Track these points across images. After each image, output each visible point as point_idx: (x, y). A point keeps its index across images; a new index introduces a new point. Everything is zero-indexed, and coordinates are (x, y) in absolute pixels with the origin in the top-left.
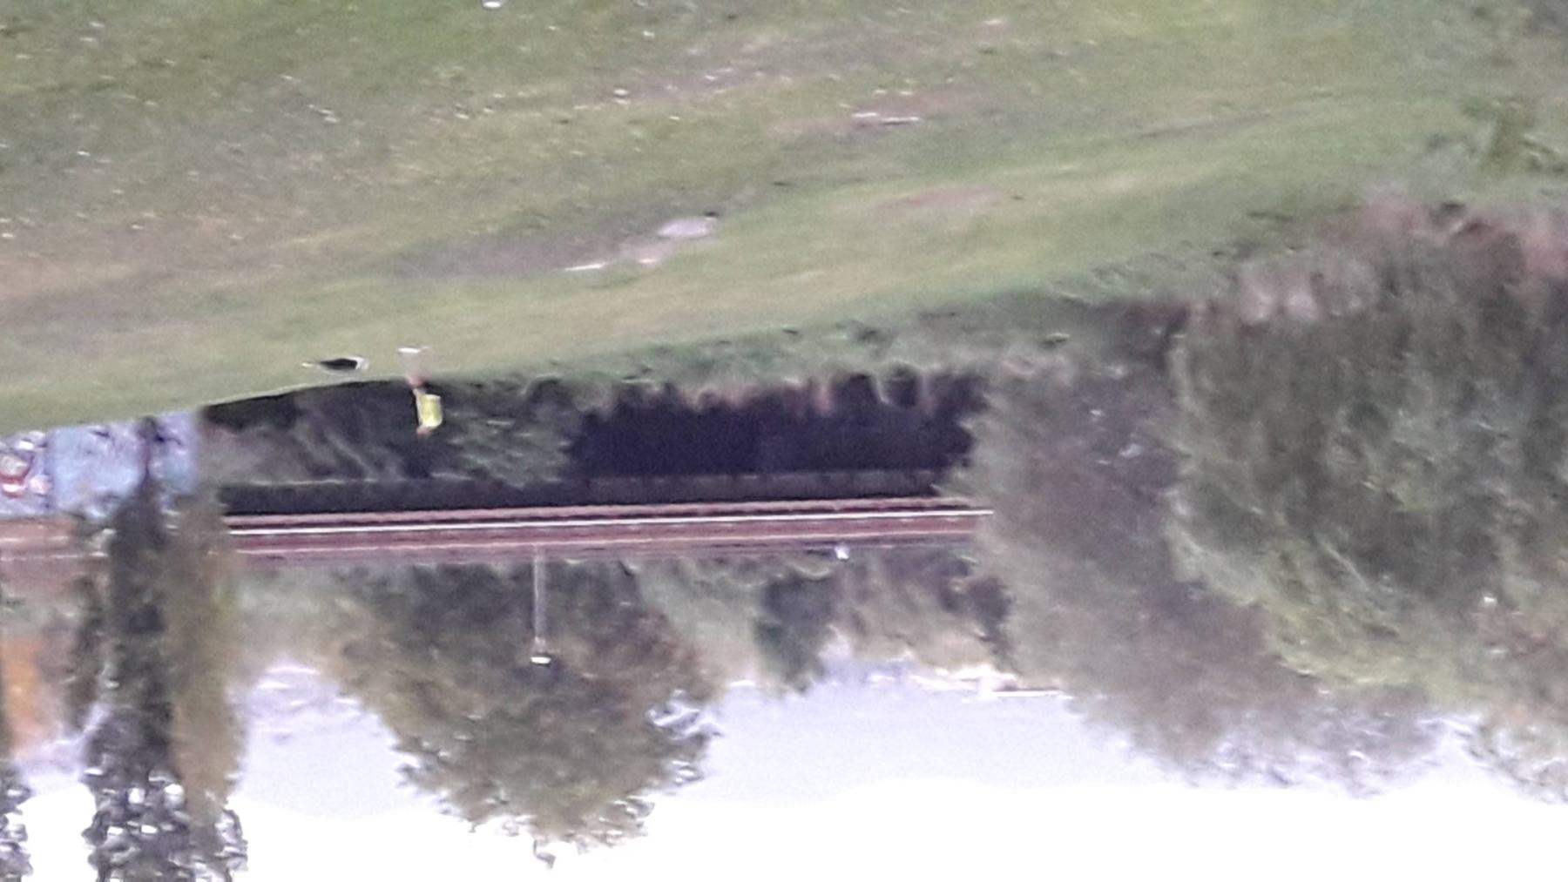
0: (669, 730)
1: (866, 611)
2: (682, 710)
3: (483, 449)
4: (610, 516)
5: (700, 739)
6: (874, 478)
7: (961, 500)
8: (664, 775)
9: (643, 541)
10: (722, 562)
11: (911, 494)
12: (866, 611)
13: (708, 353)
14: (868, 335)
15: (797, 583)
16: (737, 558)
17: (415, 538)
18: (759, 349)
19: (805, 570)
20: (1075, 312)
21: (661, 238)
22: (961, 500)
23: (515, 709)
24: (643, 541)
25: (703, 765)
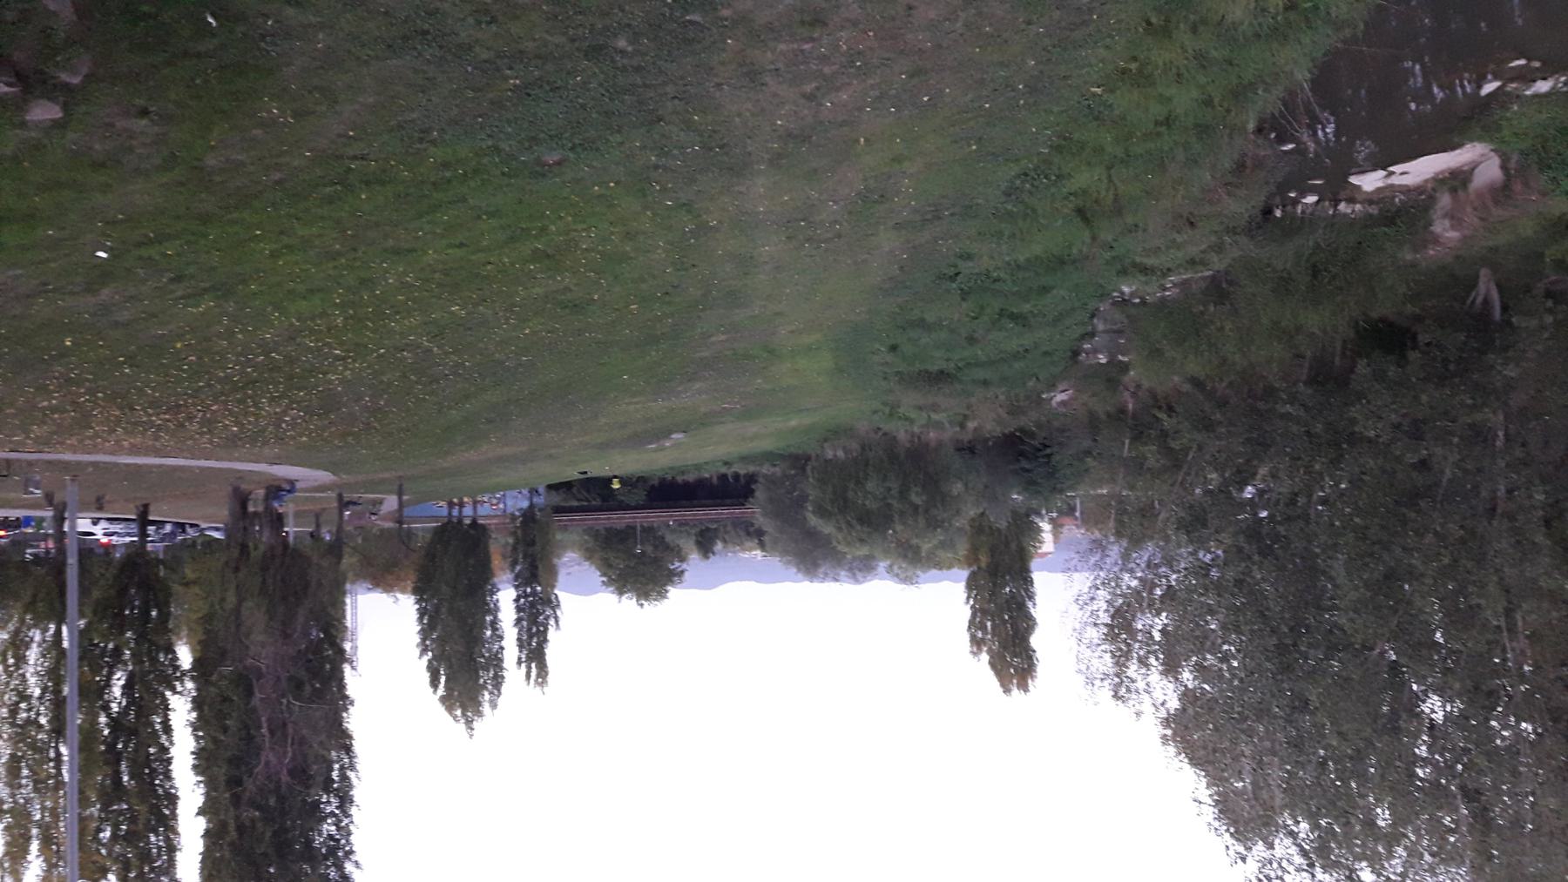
1: (726, 537)
2: (677, 564)
5: (682, 572)
6: (728, 501)
8: (672, 582)
14: (726, 463)
15: (708, 529)
16: (691, 523)
18: (698, 467)
20: (782, 457)
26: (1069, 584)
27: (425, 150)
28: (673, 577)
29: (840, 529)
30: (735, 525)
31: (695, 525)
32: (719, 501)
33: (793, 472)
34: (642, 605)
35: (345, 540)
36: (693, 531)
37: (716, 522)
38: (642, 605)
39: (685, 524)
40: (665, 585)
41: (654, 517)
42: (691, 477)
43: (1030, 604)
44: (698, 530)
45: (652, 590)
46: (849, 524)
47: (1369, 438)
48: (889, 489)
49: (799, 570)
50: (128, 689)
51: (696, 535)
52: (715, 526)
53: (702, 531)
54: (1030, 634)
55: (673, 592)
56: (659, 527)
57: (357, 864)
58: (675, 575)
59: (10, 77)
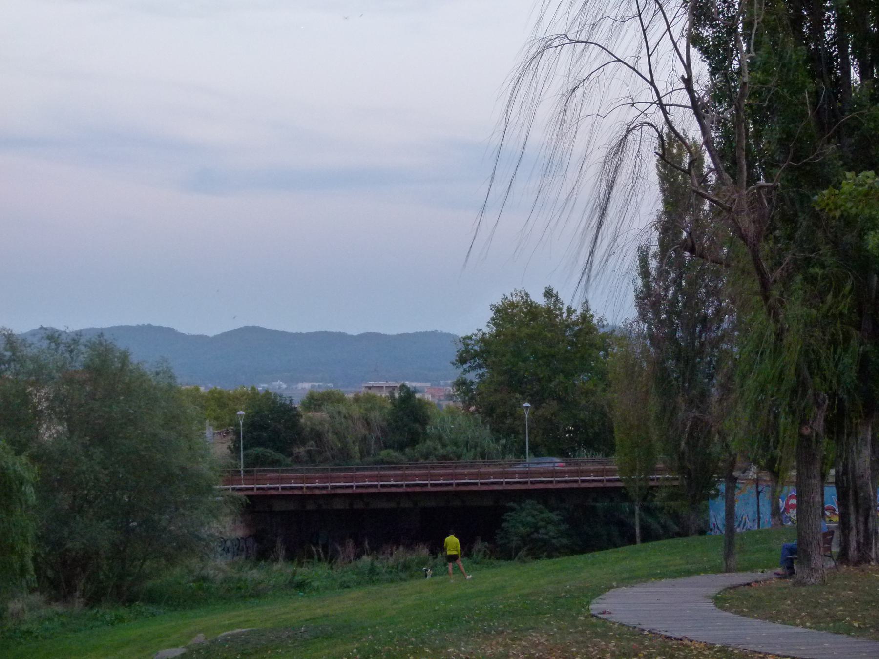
0: (480, 366)
1: (362, 431)
2: (472, 376)
3: (549, 522)
4: (480, 484)
5: (462, 360)
6: (338, 505)
7: (237, 494)
8: (483, 340)
9: (459, 471)
10: (445, 458)
11: (414, 493)
12: (362, 431)
13: (403, 575)
14: (301, 586)
15: (401, 447)
16: (433, 460)
17: (487, 475)
18: (372, 576)
19: (394, 454)
20: (154, 598)
21: (187, 648)
22: (237, 494)
23: (561, 377)
24: (459, 471)
25: (461, 346)
27: (809, 244)
30: (344, 455)
31: (426, 457)
32: (359, 505)
33: (110, 561)
35: (389, 406)
37: (382, 462)
40: (498, 334)
44: (420, 447)
45: (521, 324)
50: (369, 544)
51: (426, 436)
58: (476, 355)
59: (867, 430)
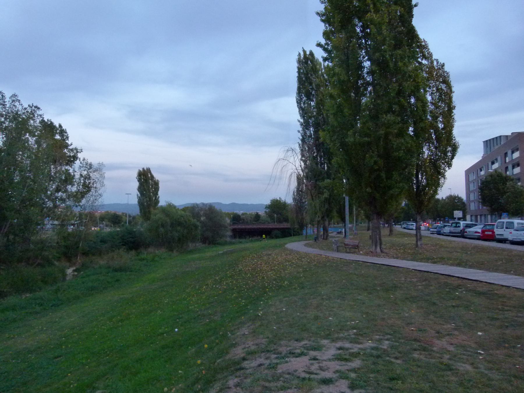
6: (247, 230)
15: (256, 221)
20: (218, 244)
26: (102, 201)
28: (268, 207)
29: (189, 220)
34: (280, 198)
36: (261, 221)
38: (280, 198)
39: (263, 223)
41: (271, 226)
42: (255, 238)
43: (139, 195)
44: (259, 221)
46: (186, 222)
47: (384, 349)
48: (171, 233)
49: (214, 207)
52: (253, 222)
53: (258, 221)
54: (139, 186)
55: (268, 202)
56: (272, 223)
57: (299, 121)
58: (268, 207)
